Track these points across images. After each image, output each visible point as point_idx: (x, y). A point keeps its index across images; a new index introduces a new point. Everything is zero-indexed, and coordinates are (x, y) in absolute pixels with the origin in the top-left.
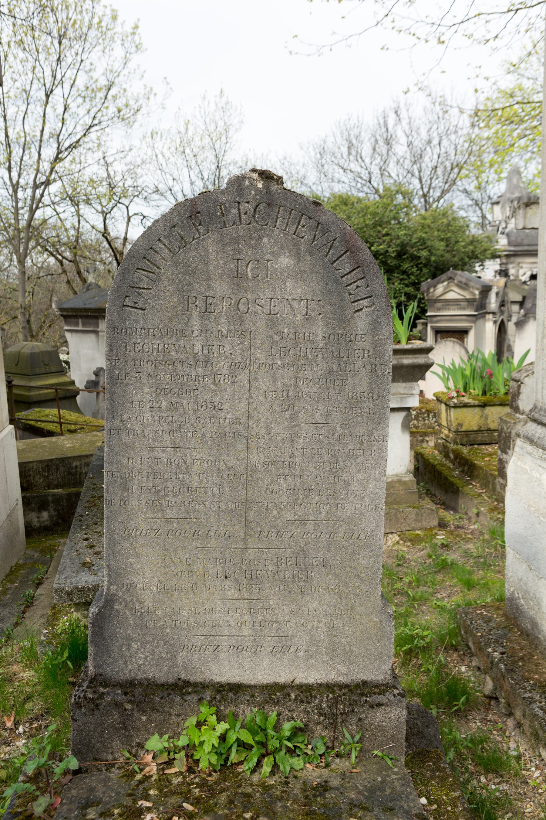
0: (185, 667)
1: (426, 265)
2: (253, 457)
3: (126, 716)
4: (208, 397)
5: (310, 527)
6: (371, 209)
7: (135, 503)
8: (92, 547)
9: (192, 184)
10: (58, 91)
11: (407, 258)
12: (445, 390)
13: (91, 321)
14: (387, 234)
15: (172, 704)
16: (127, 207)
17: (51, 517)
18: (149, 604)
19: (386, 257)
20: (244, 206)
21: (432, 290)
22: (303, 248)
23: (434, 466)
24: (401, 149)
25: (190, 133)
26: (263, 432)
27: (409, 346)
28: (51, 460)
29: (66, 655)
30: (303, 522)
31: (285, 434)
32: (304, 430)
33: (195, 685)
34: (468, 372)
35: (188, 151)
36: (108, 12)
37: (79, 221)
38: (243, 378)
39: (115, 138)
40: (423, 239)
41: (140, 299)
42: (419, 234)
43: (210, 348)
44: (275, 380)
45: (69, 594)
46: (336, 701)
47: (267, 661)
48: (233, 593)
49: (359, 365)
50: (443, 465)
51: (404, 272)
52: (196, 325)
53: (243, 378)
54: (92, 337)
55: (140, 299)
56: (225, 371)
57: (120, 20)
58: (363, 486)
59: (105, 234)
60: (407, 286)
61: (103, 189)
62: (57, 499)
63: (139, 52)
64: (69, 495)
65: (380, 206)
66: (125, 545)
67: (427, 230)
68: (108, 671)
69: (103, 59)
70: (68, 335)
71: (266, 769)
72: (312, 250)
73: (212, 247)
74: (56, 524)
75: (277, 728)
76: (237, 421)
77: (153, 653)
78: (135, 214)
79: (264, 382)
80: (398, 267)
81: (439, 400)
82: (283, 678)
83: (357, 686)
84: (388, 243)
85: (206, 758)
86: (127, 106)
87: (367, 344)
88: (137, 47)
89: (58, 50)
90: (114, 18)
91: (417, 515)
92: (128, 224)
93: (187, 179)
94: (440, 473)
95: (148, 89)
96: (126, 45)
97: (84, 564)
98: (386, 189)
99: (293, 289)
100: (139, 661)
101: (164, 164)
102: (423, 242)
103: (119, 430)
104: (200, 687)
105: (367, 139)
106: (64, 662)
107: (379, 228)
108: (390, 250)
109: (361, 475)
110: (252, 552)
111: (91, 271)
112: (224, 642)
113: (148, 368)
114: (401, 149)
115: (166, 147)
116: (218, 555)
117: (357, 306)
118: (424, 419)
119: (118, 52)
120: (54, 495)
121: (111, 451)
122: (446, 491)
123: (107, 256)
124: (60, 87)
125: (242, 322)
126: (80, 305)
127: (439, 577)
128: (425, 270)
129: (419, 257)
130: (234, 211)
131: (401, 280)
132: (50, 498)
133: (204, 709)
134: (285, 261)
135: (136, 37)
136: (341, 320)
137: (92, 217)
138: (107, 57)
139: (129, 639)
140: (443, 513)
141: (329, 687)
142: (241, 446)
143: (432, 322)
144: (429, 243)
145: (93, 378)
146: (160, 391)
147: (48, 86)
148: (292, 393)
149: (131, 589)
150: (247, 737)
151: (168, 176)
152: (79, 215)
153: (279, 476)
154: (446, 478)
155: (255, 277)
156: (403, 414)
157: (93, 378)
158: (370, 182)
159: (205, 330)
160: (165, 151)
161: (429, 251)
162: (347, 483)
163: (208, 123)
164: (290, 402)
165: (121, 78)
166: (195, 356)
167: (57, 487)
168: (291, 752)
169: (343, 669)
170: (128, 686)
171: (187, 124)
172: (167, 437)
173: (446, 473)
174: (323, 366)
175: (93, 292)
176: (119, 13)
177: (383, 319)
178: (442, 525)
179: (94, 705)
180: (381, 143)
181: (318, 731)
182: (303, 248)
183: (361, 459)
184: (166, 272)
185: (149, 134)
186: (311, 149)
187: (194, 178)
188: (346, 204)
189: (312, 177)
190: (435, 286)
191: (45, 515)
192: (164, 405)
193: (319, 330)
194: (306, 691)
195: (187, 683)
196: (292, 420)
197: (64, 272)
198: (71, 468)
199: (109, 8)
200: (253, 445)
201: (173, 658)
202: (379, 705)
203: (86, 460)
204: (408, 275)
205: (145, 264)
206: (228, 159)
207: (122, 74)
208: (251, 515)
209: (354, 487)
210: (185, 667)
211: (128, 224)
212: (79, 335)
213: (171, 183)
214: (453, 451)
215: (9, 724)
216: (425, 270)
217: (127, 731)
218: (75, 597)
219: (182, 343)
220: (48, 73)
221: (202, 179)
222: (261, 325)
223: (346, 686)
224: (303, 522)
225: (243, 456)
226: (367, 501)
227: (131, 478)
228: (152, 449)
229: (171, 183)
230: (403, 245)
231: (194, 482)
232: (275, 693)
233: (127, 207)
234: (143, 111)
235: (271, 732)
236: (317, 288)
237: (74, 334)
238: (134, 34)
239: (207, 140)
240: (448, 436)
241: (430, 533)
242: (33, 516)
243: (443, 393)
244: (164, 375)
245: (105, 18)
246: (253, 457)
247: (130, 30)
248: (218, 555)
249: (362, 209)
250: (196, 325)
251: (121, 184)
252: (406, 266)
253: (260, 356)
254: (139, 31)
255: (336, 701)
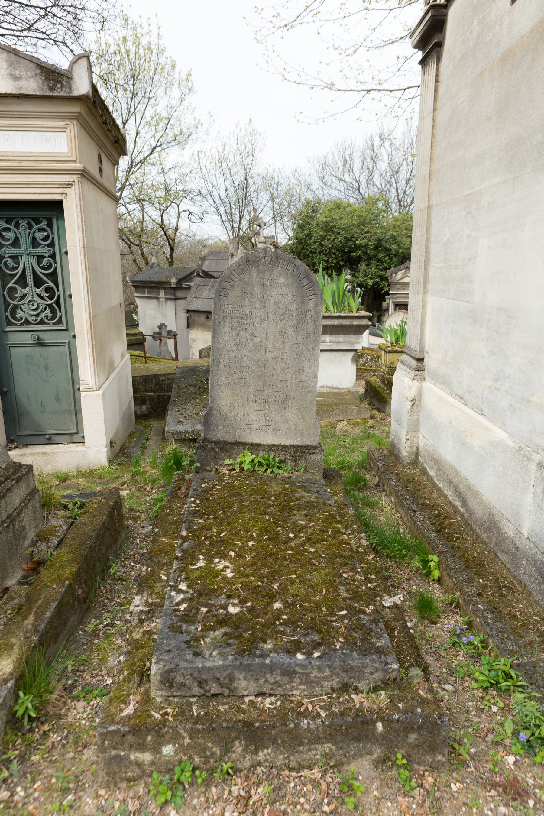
0: (239, 437)
1: (395, 256)
2: (268, 355)
3: (216, 453)
4: (251, 332)
5: (289, 383)
6: (357, 213)
7: (222, 372)
8: (182, 414)
9: (227, 191)
10: (131, 121)
11: (382, 250)
12: (385, 343)
13: (154, 290)
14: (368, 232)
15: (234, 450)
16: (178, 206)
17: (148, 409)
18: (226, 411)
19: (366, 248)
20: (267, 258)
21: (394, 275)
22: (289, 275)
23: (375, 388)
24: (383, 165)
25: (226, 152)
26: (272, 346)
27: (357, 314)
28: (148, 376)
29: (172, 462)
30: (286, 381)
31: (280, 347)
32: (287, 346)
33: (243, 444)
34: (399, 332)
35: (224, 165)
36: (169, 62)
37: (143, 215)
38: (264, 325)
39: (172, 156)
40: (394, 236)
41: (226, 293)
42: (392, 232)
43: (252, 313)
44: (277, 326)
45: (173, 434)
46: (297, 451)
47: (271, 435)
48: (258, 408)
49: (309, 321)
50: (380, 387)
51: (379, 260)
52: (247, 303)
53: (264, 325)
54: (155, 302)
55: (226, 293)
56: (258, 321)
57: (177, 69)
58: (310, 368)
59: (162, 226)
60: (381, 270)
61: (161, 193)
62: (151, 399)
63: (191, 94)
64: (158, 396)
65: (364, 210)
66: (217, 388)
67: (397, 229)
68: (209, 437)
69: (165, 98)
70: (138, 300)
71: (269, 471)
72: (293, 276)
73: (254, 274)
74: (151, 413)
75: (274, 459)
76: (262, 341)
77: (226, 430)
78: (184, 211)
79: (272, 327)
80: (375, 256)
81: (380, 348)
82: (277, 442)
83: (305, 447)
84: (369, 238)
85: (246, 466)
86: (181, 132)
87: (313, 313)
88: (190, 90)
89: (132, 89)
90: (173, 67)
91: (358, 411)
92: (178, 218)
93: (223, 187)
94: (378, 392)
95: (197, 121)
96: (182, 88)
97: (179, 421)
98: (370, 198)
99: (285, 290)
100: (222, 434)
101: (207, 175)
102: (394, 238)
103: (216, 343)
104: (244, 444)
105: (357, 157)
106: (172, 465)
107: (362, 227)
108: (370, 243)
109: (309, 364)
110: (266, 392)
111: (154, 254)
112: (254, 427)
113: (228, 319)
114: (383, 165)
115: (208, 162)
116: (253, 393)
117: (309, 298)
118: (375, 362)
119: (176, 93)
120: (149, 396)
121: (213, 351)
122: (381, 402)
123: (162, 240)
124: (133, 117)
125: (265, 303)
126: (146, 279)
127: (365, 441)
128: (394, 259)
129: (391, 250)
130: (263, 260)
131: (377, 266)
132: (147, 398)
133: (246, 451)
134: (282, 280)
135: (190, 84)
136: (303, 303)
137: (153, 212)
138: (168, 97)
139: (217, 424)
140: (375, 412)
141: (294, 446)
142: (263, 351)
143: (393, 298)
144: (399, 239)
145: (158, 330)
146: (232, 328)
147: (124, 117)
148: (283, 331)
149: (219, 405)
150: (262, 461)
151: (209, 184)
152: (142, 209)
153: (277, 363)
154: (381, 395)
155: (270, 286)
156: (352, 354)
157: (158, 330)
158: (359, 190)
159: (251, 306)
160: (208, 166)
161: (398, 245)
162: (304, 367)
163: (239, 144)
164: (282, 334)
165: (178, 113)
166: (246, 315)
167: (151, 392)
168: (279, 468)
169: (300, 440)
170: (217, 443)
171: (224, 145)
172: (235, 347)
173: (381, 391)
174: (296, 321)
175: (155, 269)
176: (177, 63)
177: (319, 303)
178: (372, 417)
179: (204, 448)
180: (369, 160)
181: (289, 462)
182: (289, 275)
183: (309, 358)
184: (236, 283)
185: (196, 153)
186: (316, 163)
187: (229, 187)
188: (339, 208)
189: (316, 184)
190: (396, 273)
191: (144, 407)
192: (234, 334)
193: (294, 307)
194: (285, 448)
195: (239, 443)
196: (283, 341)
197: (132, 253)
198: (159, 380)
199: (169, 59)
200: (268, 351)
201: (234, 433)
202: (313, 453)
203: (168, 377)
204: (382, 263)
205: (229, 280)
206: (254, 171)
207: (178, 110)
208: (266, 378)
209: (306, 369)
210: (239, 437)
211: (178, 218)
212: (145, 300)
213: (211, 188)
214: (387, 379)
215: (148, 489)
216: (394, 259)
217: (216, 459)
218: (176, 436)
219: (241, 310)
220: (124, 106)
221: (234, 187)
222: (272, 304)
223: (301, 446)
224: (286, 381)
225: (264, 355)
226: (311, 374)
227: (220, 362)
228: (229, 351)
229: (211, 189)
230: (379, 240)
231: (244, 364)
232: (273, 448)
233: (178, 206)
234: (193, 137)
235: (271, 460)
236: (294, 291)
237: (142, 300)
238: (187, 80)
239: (239, 158)
240: (385, 370)
241: (365, 420)
242: (138, 407)
243: (384, 344)
244: (234, 322)
245: (167, 67)
246: (268, 355)
247: (185, 77)
248: (253, 393)
249: (351, 212)
250: (247, 303)
251: (174, 188)
252: (381, 255)
253: (271, 316)
254: (191, 78)
255: (297, 451)
